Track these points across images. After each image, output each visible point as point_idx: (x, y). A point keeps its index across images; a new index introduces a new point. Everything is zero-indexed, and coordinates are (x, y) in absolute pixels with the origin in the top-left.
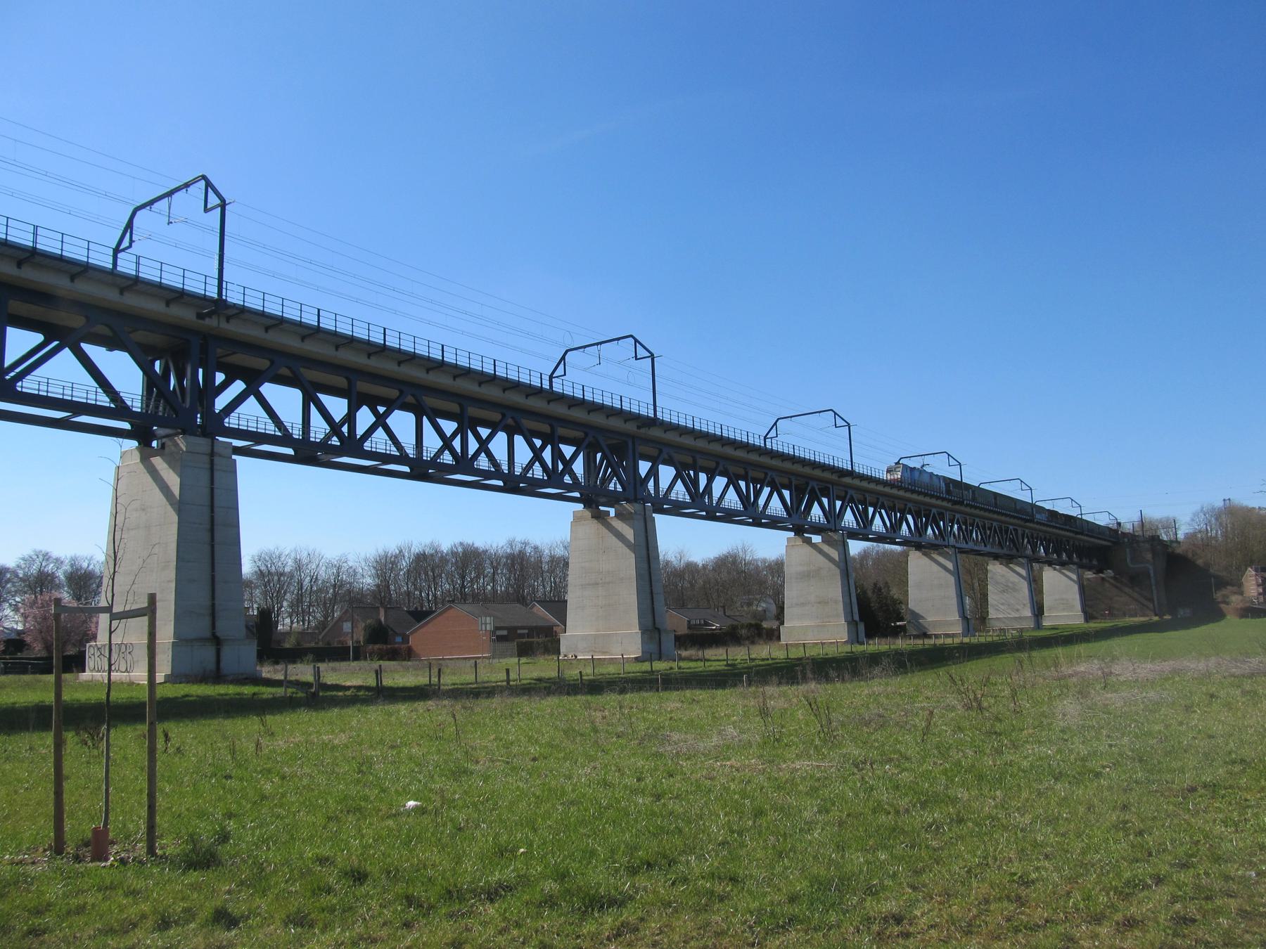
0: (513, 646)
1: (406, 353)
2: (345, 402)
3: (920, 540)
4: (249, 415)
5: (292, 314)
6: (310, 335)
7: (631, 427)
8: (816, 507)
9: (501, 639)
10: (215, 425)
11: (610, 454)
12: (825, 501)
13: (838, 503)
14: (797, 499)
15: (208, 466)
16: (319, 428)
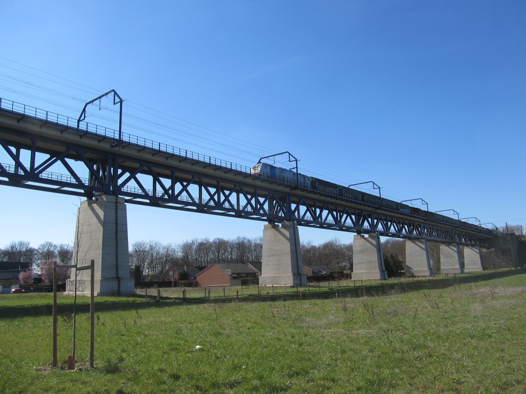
0: (240, 281)
4: (132, 186)
6: (142, 150)
8: (366, 222)
9: (234, 278)
10: (118, 191)
12: (370, 220)
14: (358, 219)
15: (115, 207)
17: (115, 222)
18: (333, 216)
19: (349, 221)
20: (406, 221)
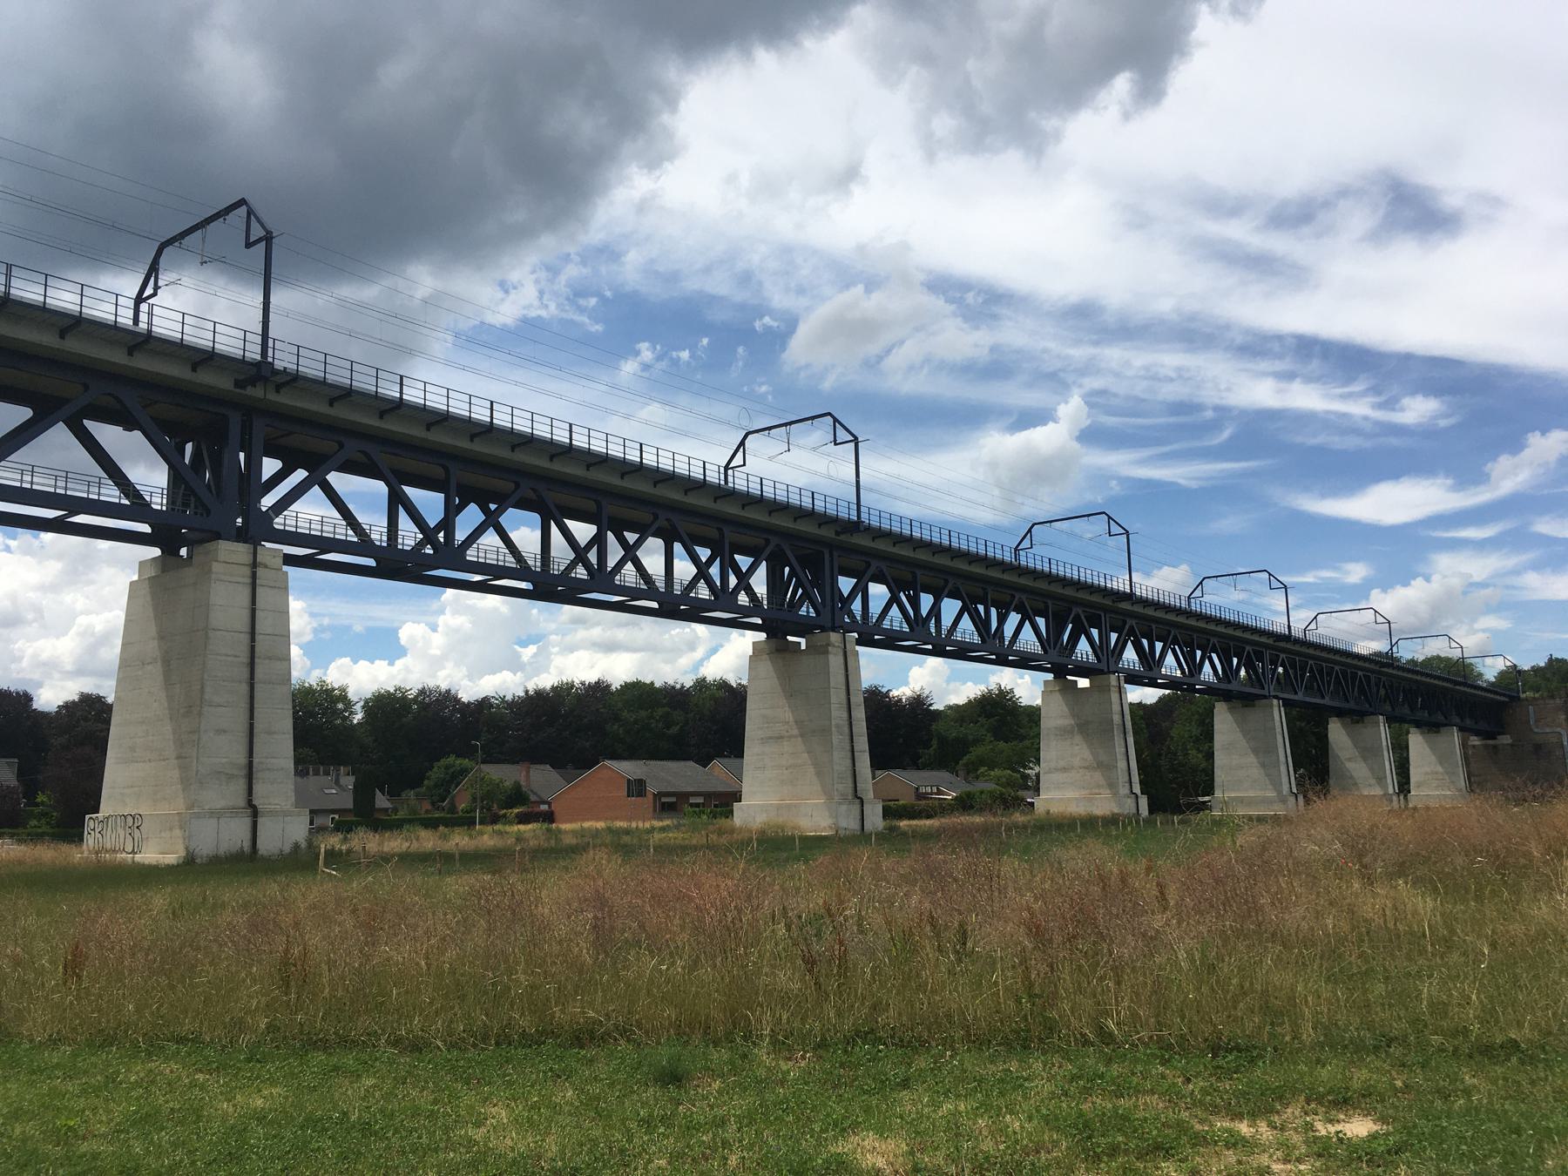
1: (521, 435)
2: (439, 497)
3: (1229, 687)
4: (312, 513)
5: (459, 408)
6: (438, 422)
7: (827, 533)
8: (1083, 640)
10: (258, 529)
11: (807, 566)
12: (1095, 632)
13: (1114, 636)
14: (1056, 627)
15: (248, 580)
16: (409, 535)
17: (247, 628)
18: (975, 618)
19: (1027, 633)
20: (1214, 640)
